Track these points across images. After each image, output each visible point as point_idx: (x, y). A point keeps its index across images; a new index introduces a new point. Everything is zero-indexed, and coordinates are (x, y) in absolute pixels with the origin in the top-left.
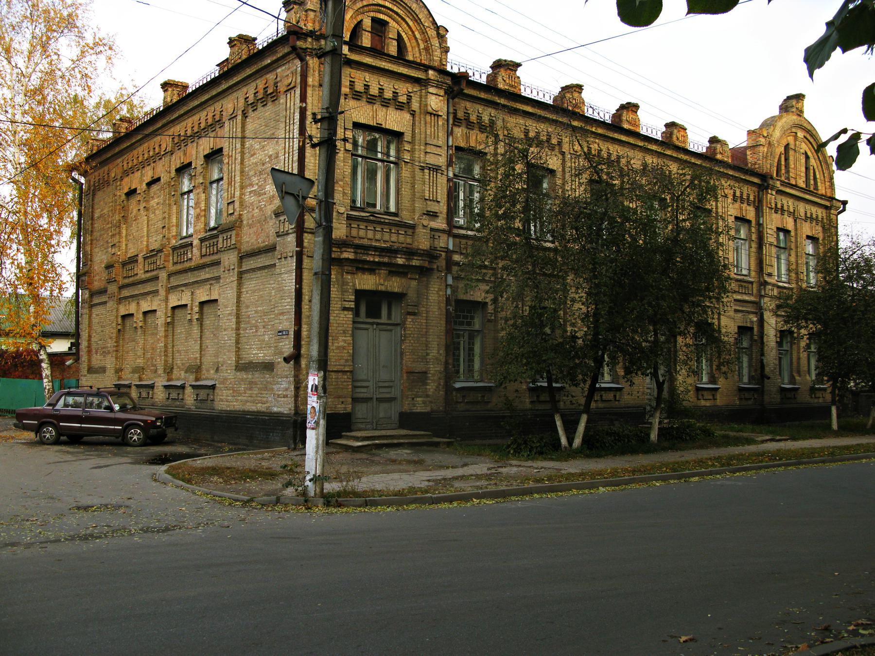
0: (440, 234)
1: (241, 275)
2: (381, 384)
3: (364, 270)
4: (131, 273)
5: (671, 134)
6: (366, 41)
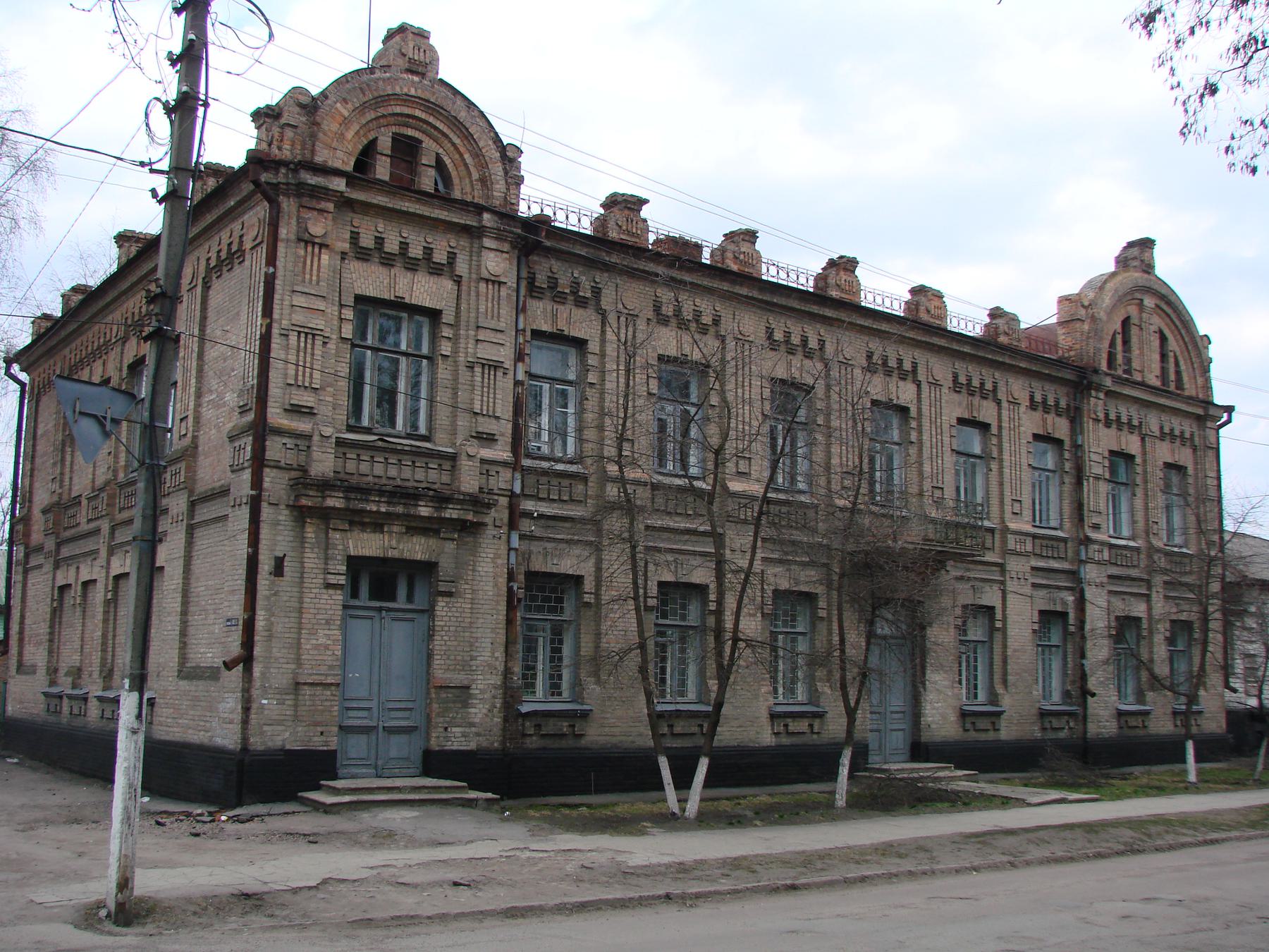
0: (500, 469)
1: (191, 530)
2: (391, 705)
3: (363, 526)
4: (73, 522)
5: (917, 304)
6: (382, 170)
